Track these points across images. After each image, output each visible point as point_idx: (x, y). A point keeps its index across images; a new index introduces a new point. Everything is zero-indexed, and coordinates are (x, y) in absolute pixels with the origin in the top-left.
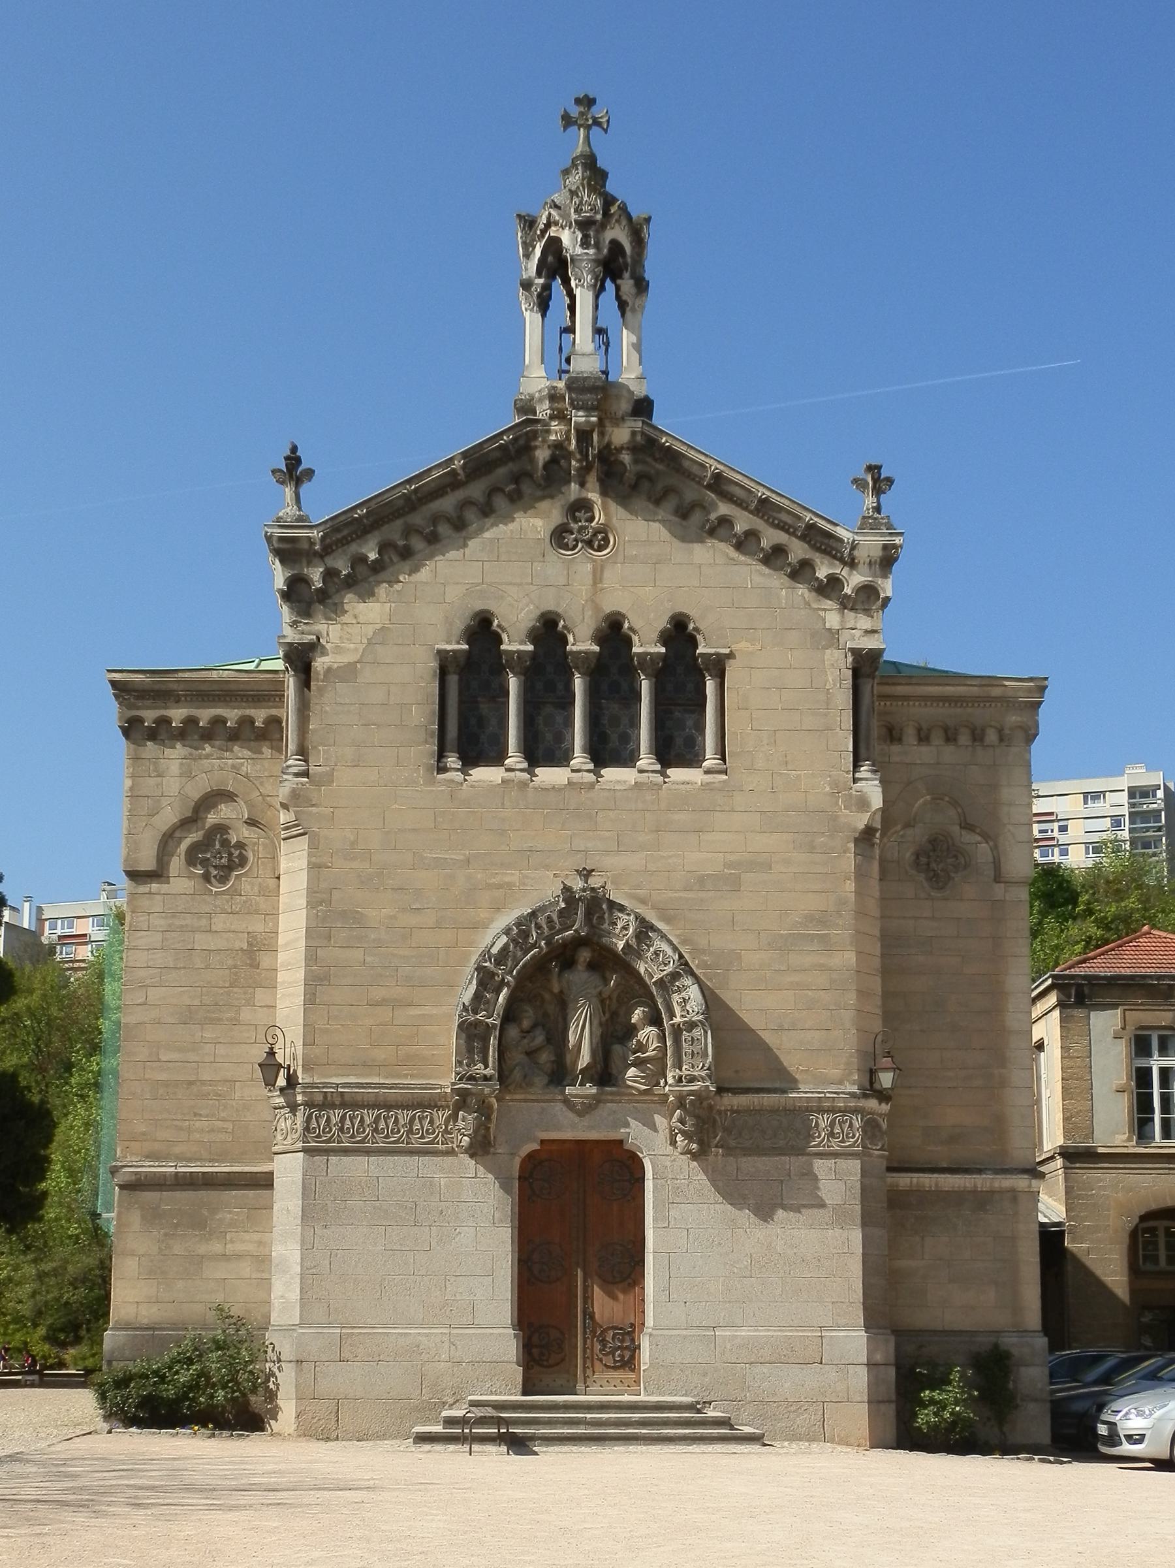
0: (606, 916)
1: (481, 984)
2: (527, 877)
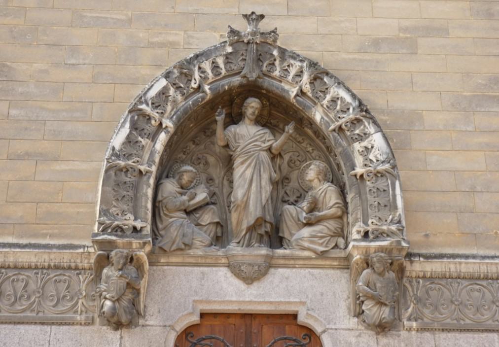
0: (277, 63)
1: (134, 127)
2: (192, 37)
